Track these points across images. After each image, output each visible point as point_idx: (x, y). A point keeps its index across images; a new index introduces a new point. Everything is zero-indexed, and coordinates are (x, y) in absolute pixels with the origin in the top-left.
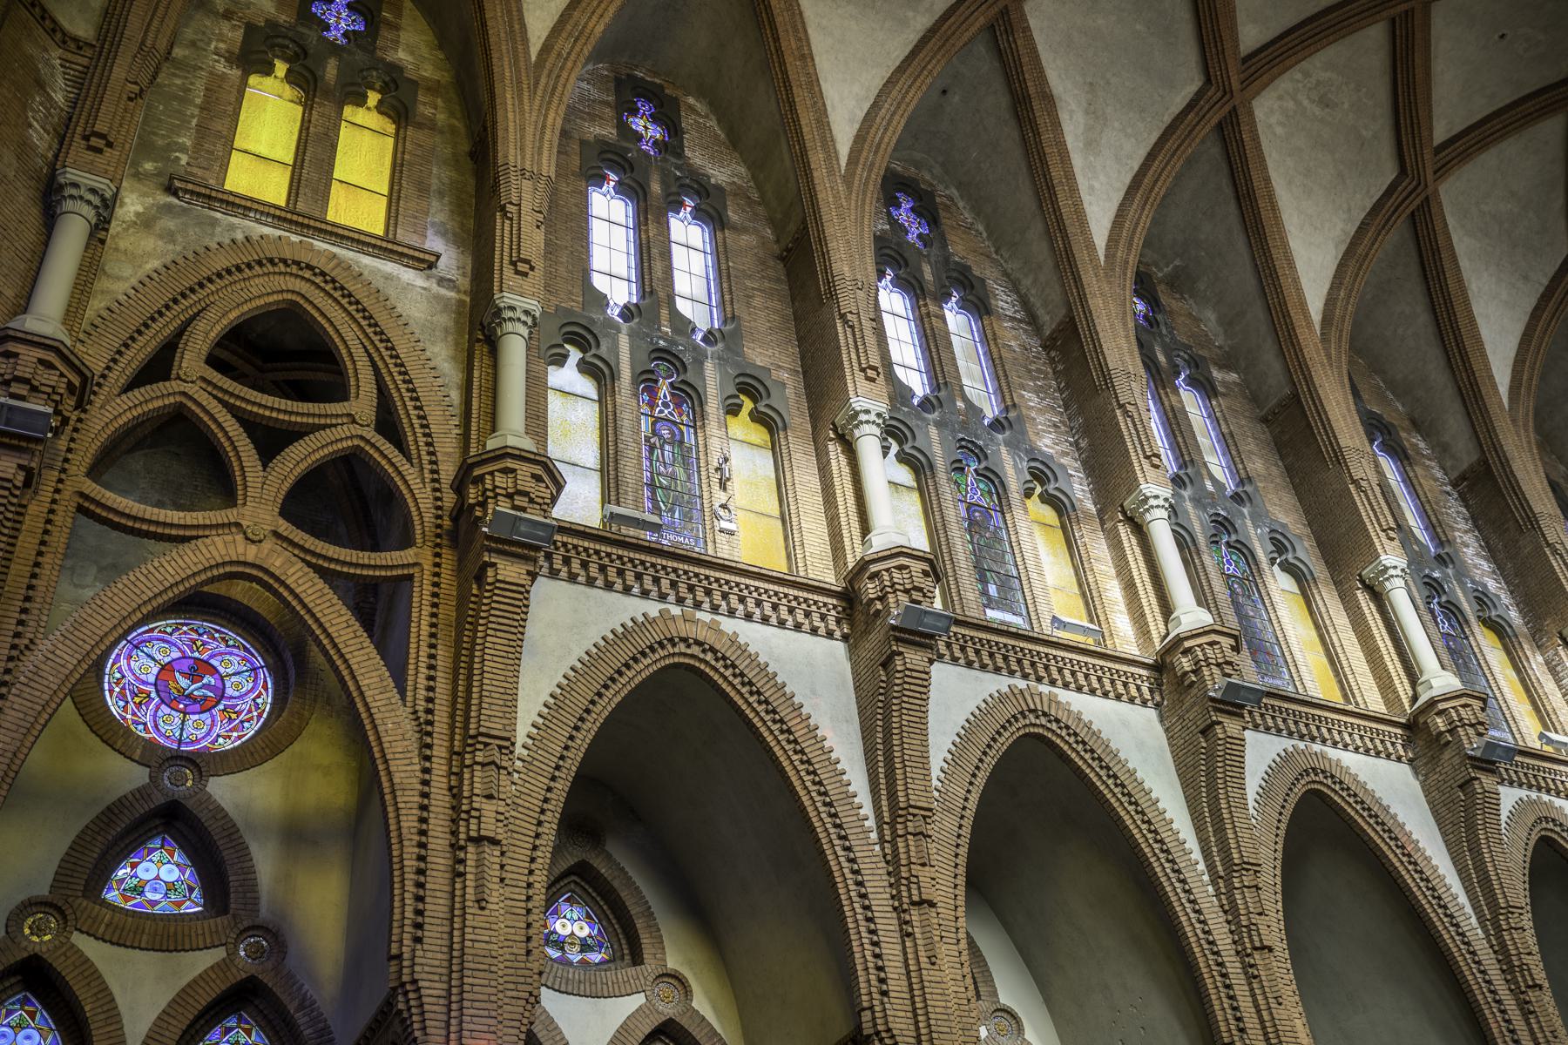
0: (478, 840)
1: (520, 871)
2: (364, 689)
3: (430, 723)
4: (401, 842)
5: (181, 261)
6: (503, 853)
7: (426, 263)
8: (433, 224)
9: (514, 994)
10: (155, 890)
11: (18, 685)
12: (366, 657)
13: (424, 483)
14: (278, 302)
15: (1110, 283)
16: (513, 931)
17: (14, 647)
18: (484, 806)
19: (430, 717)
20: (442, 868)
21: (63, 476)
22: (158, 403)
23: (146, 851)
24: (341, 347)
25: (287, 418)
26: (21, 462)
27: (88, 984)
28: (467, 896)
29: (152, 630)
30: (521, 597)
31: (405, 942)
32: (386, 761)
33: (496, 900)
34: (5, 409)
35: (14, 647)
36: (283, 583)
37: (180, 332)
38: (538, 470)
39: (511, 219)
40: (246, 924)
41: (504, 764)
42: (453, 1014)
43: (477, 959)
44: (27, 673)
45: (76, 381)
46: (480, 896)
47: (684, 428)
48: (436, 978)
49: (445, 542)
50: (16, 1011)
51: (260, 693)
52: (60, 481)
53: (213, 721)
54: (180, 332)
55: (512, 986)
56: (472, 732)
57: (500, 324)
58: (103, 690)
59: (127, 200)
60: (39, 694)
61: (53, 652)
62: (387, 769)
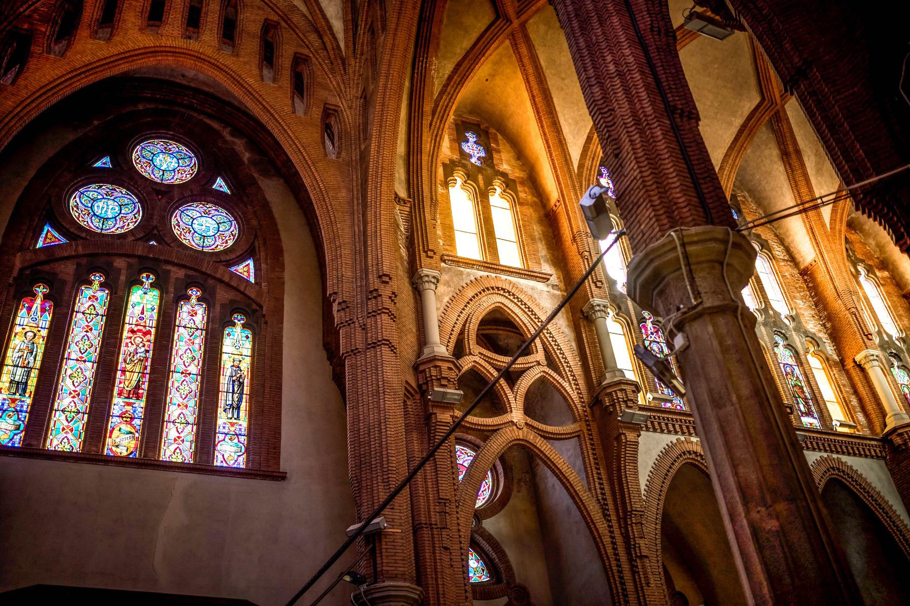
7: (544, 279)
15: (835, 243)
36: (535, 447)
39: (587, 259)
47: (662, 344)
57: (594, 313)
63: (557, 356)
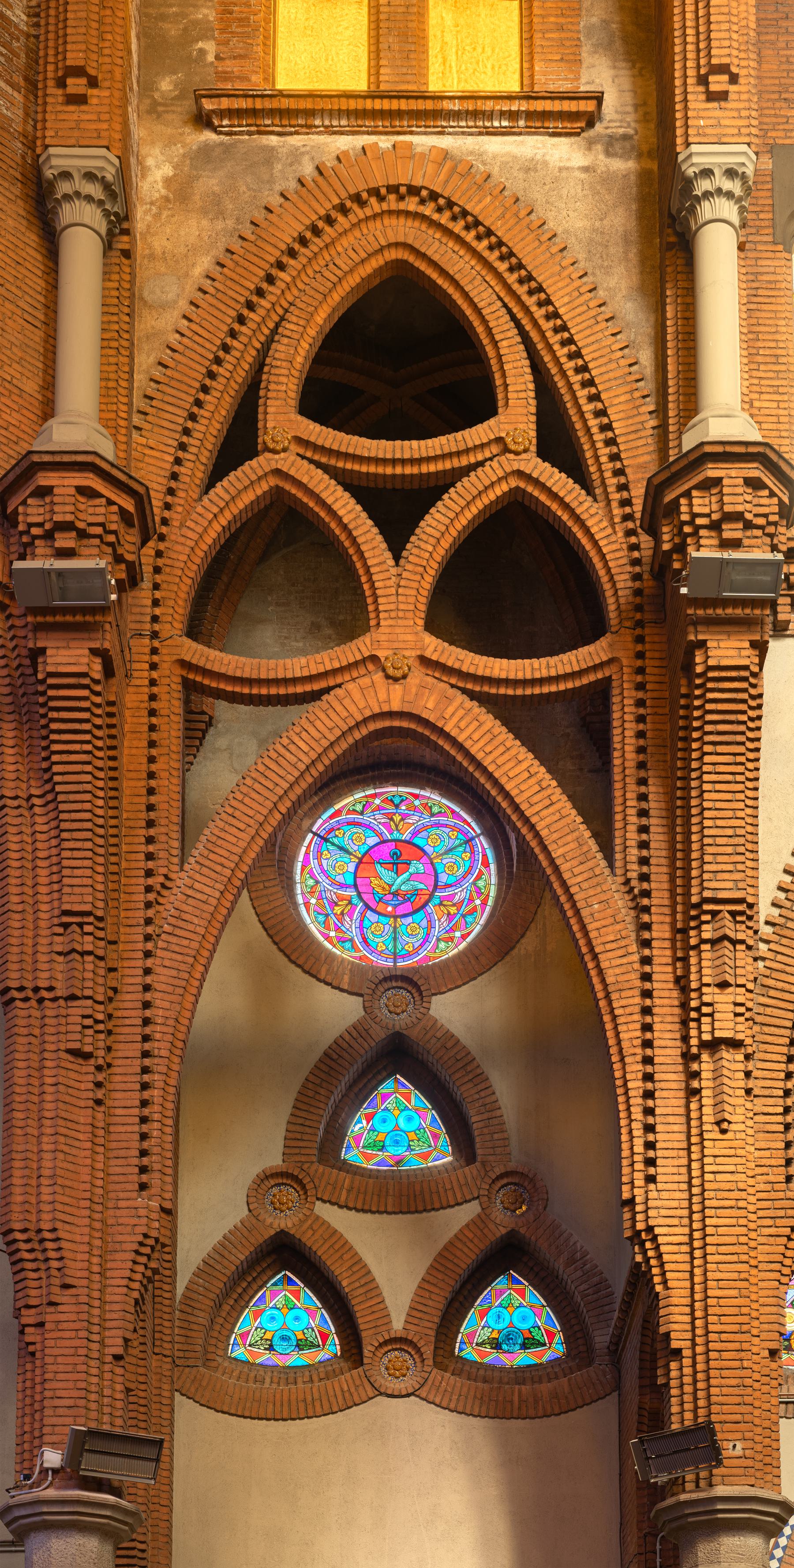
0: (714, 1045)
1: (774, 1075)
2: (558, 862)
3: (646, 894)
4: (622, 1060)
5: (236, 245)
6: (748, 1057)
8: (589, 33)
9: (772, 1231)
10: (397, 1143)
11: (164, 936)
12: (558, 816)
13: (613, 525)
14: (379, 271)
16: (767, 1153)
17: (149, 889)
18: (717, 998)
19: (645, 885)
20: (674, 1085)
21: (156, 643)
22: (248, 498)
23: (379, 1098)
24: (476, 323)
25: (415, 470)
26: (94, 645)
27: (341, 1257)
28: (705, 1118)
29: (338, 813)
30: (745, 685)
31: (637, 1183)
32: (595, 957)
33: (742, 1118)
34: (54, 577)
35: (149, 889)
36: (441, 732)
37: (259, 367)
38: (754, 470)
40: (498, 1171)
41: (740, 936)
42: (697, 1262)
43: (721, 1195)
44: (170, 919)
45: (129, 505)
46: (719, 1117)
48: (675, 1221)
49: (648, 616)
50: (280, 1291)
51: (481, 873)
52: (154, 651)
53: (429, 921)
54: (259, 367)
55: (769, 1222)
56: (695, 899)
58: (295, 905)
59: (150, 162)
60: (185, 942)
61: (191, 887)
62: (598, 966)
63: (579, 407)
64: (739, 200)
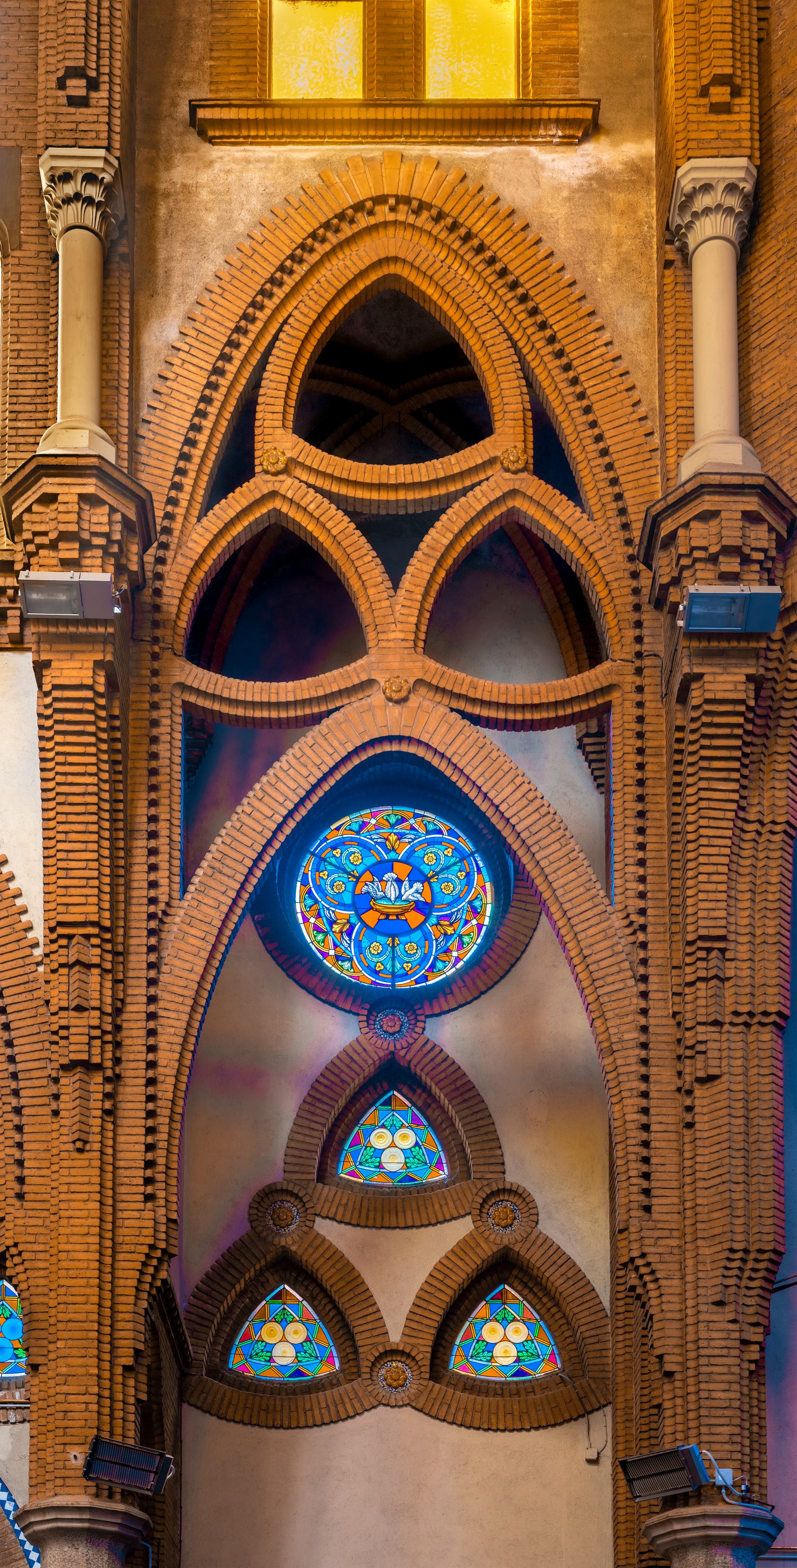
64: (99, 205)
